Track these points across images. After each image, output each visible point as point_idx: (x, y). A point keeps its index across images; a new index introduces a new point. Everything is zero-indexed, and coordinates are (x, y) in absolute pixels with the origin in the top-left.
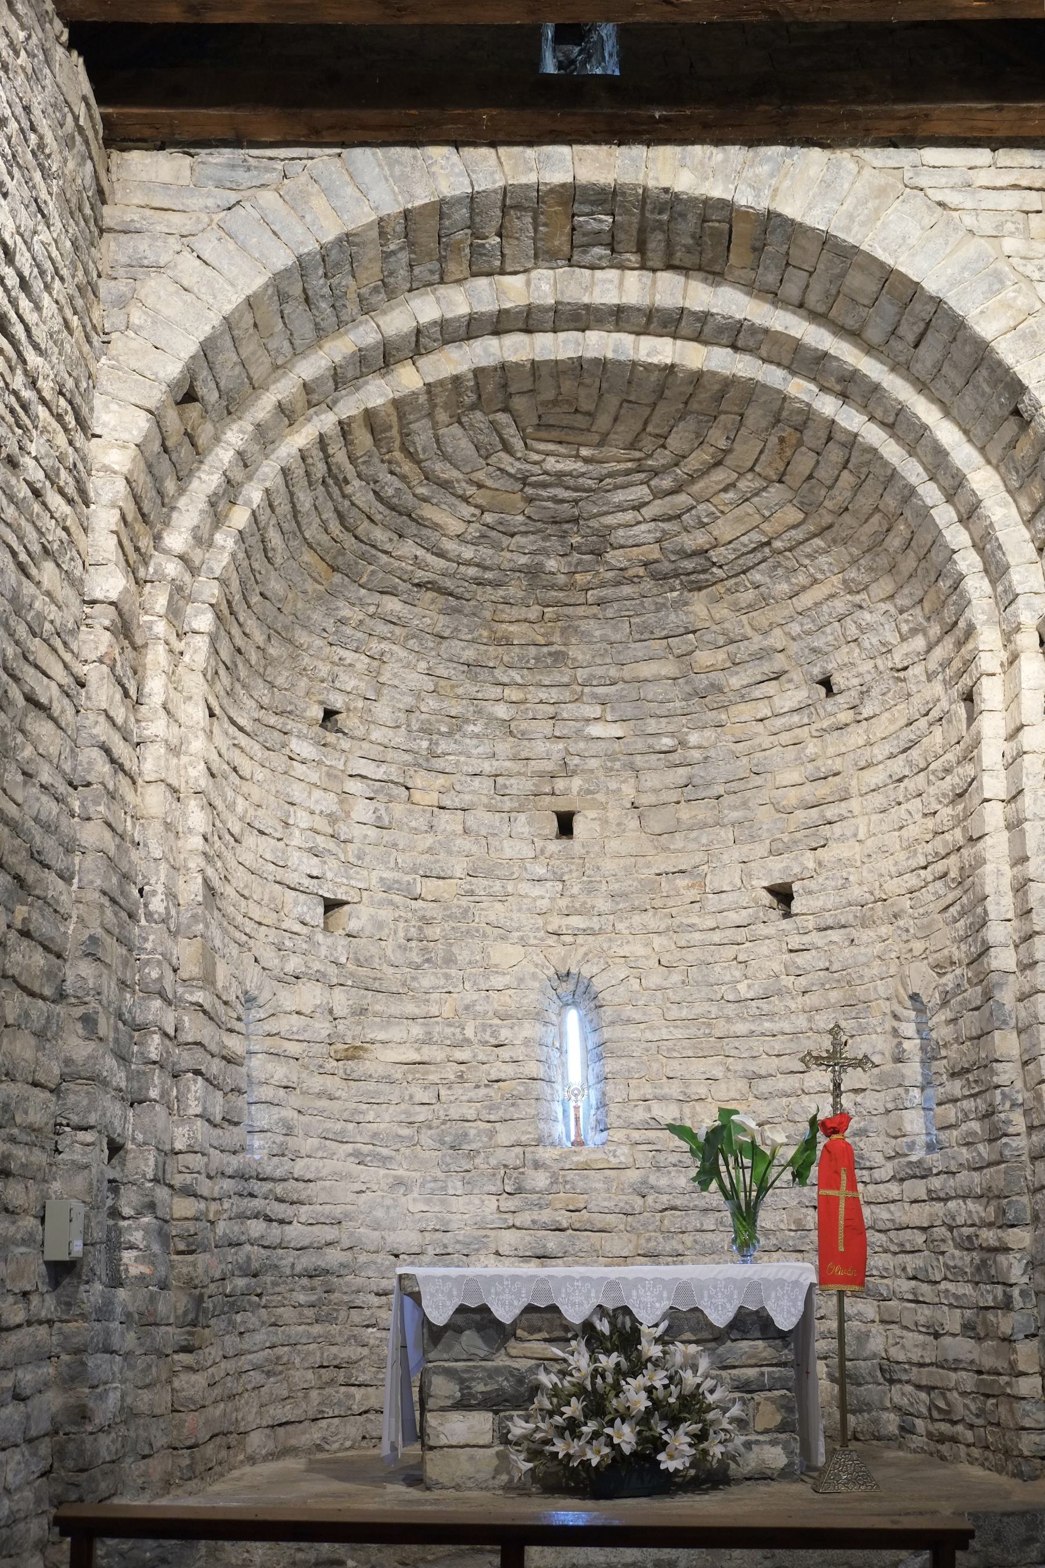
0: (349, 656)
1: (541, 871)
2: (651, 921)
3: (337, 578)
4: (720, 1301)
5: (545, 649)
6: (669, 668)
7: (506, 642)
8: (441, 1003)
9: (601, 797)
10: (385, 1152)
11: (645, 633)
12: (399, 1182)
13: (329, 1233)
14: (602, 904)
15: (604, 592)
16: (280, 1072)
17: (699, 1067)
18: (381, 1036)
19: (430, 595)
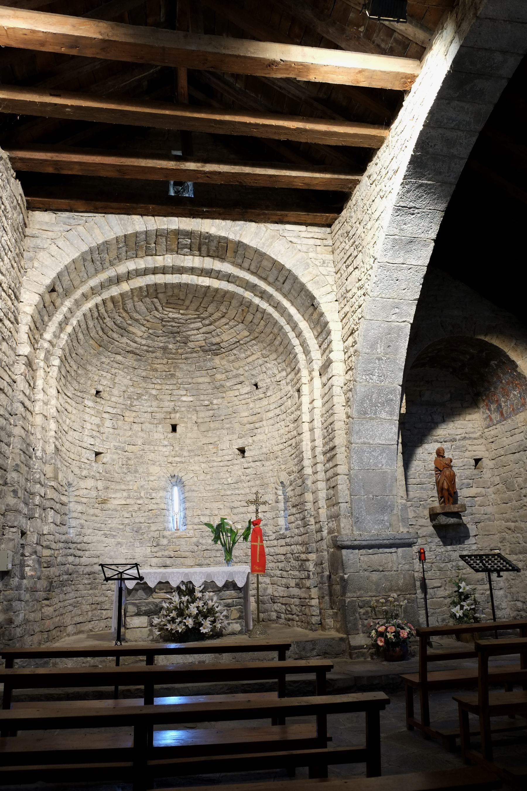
0: (105, 374)
1: (166, 443)
2: (201, 459)
3: (101, 349)
5: (168, 373)
6: (207, 380)
8: (133, 485)
9: (185, 420)
10: (114, 533)
11: (200, 369)
12: (119, 543)
14: (185, 453)
15: (187, 355)
16: (80, 508)
17: (215, 505)
19: (131, 355)
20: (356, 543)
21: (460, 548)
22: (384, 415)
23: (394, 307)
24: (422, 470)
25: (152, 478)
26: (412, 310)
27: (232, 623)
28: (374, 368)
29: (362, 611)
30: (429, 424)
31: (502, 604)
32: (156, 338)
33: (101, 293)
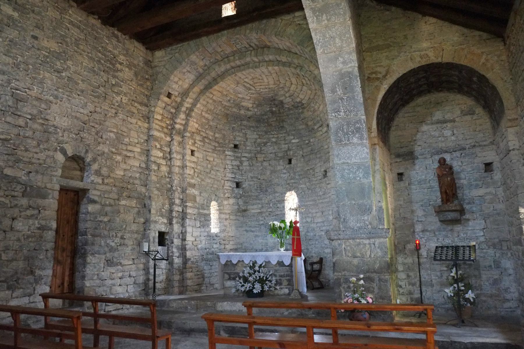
0: (238, 134)
1: (285, 171)
8: (265, 200)
22: (355, 140)
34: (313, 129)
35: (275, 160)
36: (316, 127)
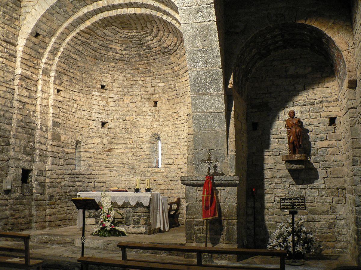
0: (105, 75)
1: (150, 113)
2: (170, 123)
3: (97, 61)
4: (133, 200)
5: (146, 69)
6: (170, 71)
7: (139, 69)
8: (129, 140)
9: (162, 98)
10: (117, 169)
11: (164, 65)
12: (120, 175)
13: (103, 184)
14: (161, 120)
15: (154, 57)
16: (88, 155)
17: (176, 152)
18: (116, 147)
19: (120, 61)
20: (194, 182)
21: (309, 186)
22: (212, 91)
23: (198, 12)
24: (283, 128)
25: (142, 136)
26: (213, 11)
27: (141, 227)
28: (198, 58)
29: (196, 228)
30: (292, 92)
31: (343, 230)
32: (131, 49)
33: (76, 30)
34: (179, 75)
35: (141, 102)
36: (181, 73)
